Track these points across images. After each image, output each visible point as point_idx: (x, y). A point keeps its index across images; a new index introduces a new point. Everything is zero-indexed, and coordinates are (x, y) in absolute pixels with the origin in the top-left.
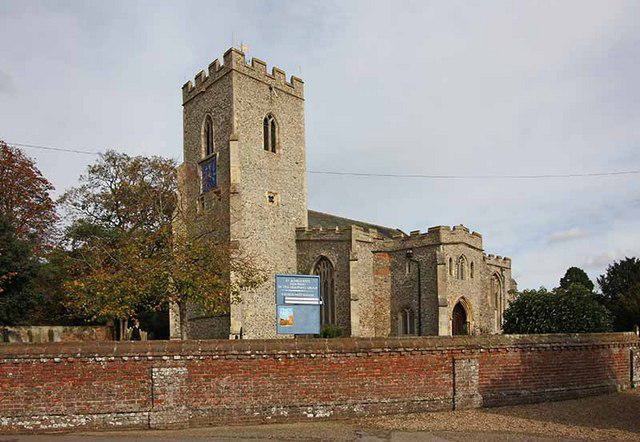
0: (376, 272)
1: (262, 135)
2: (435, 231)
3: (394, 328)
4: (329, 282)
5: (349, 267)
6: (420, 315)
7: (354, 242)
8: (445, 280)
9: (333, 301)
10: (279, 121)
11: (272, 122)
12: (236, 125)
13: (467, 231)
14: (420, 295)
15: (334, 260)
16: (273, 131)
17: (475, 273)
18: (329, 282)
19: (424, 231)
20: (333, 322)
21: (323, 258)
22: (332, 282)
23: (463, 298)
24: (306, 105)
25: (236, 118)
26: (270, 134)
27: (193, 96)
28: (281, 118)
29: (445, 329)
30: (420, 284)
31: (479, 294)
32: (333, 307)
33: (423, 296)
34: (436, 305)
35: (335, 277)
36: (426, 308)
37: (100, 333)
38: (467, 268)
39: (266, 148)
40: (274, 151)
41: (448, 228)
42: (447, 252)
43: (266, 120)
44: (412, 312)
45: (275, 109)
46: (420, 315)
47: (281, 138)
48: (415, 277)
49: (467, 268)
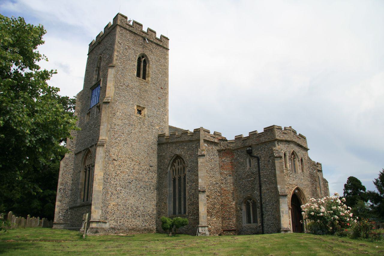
0: (221, 167)
1: (136, 67)
2: (270, 130)
3: (239, 218)
4: (182, 177)
5: (197, 163)
6: (261, 205)
7: (202, 141)
8: (282, 172)
9: (185, 194)
10: (150, 59)
11: (145, 61)
12: (115, 58)
13: (295, 132)
14: (260, 186)
15: (187, 158)
16: (145, 66)
17: (305, 167)
18: (182, 177)
19: (260, 130)
20: (185, 212)
21: (178, 157)
22: (185, 176)
23: (298, 189)
24: (170, 52)
25: (116, 53)
26: (182, 199)
27: (94, 48)
28: (151, 58)
29: (286, 221)
30: (260, 176)
31: (310, 186)
32: (185, 198)
33: (263, 187)
34: (277, 196)
35: (187, 172)
36: (266, 198)
37: (71, 241)
38: (298, 164)
39: (138, 75)
40: (144, 78)
41: (280, 128)
42: (280, 148)
43: (139, 59)
44: (254, 203)
45: (147, 53)
46: (261, 205)
47: (150, 72)
48: (255, 170)
49: (298, 164)
